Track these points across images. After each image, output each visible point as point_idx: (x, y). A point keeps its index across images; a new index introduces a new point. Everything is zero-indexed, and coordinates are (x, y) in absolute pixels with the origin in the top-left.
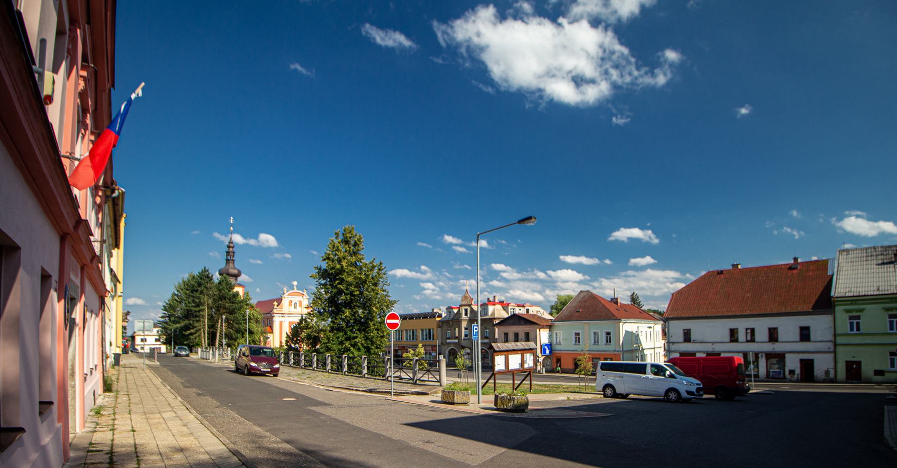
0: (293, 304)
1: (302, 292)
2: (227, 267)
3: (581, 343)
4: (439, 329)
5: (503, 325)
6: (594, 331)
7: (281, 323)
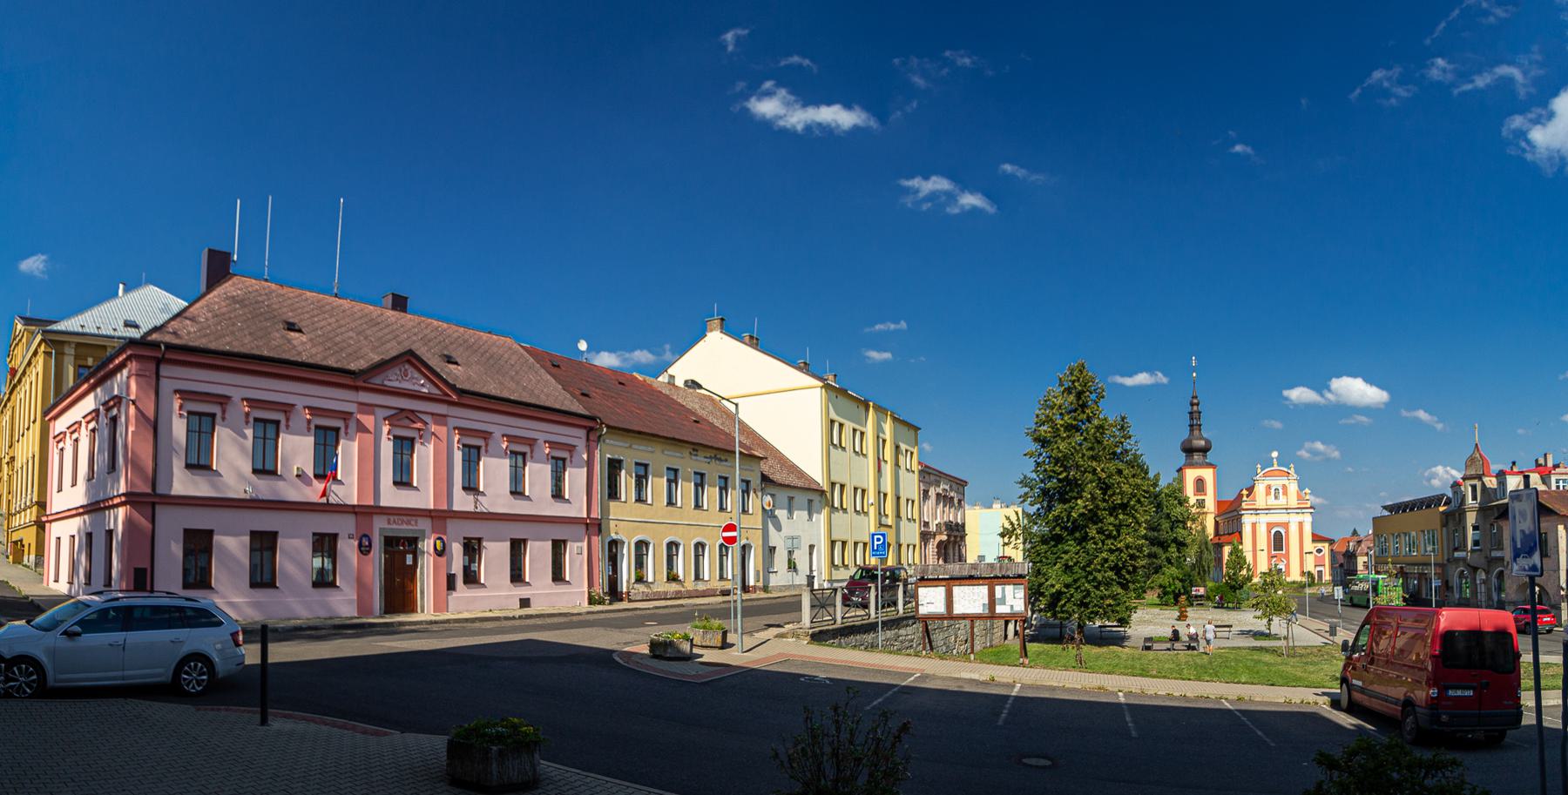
1: (1286, 470)
2: (1191, 437)
4: (1444, 529)
7: (1254, 525)
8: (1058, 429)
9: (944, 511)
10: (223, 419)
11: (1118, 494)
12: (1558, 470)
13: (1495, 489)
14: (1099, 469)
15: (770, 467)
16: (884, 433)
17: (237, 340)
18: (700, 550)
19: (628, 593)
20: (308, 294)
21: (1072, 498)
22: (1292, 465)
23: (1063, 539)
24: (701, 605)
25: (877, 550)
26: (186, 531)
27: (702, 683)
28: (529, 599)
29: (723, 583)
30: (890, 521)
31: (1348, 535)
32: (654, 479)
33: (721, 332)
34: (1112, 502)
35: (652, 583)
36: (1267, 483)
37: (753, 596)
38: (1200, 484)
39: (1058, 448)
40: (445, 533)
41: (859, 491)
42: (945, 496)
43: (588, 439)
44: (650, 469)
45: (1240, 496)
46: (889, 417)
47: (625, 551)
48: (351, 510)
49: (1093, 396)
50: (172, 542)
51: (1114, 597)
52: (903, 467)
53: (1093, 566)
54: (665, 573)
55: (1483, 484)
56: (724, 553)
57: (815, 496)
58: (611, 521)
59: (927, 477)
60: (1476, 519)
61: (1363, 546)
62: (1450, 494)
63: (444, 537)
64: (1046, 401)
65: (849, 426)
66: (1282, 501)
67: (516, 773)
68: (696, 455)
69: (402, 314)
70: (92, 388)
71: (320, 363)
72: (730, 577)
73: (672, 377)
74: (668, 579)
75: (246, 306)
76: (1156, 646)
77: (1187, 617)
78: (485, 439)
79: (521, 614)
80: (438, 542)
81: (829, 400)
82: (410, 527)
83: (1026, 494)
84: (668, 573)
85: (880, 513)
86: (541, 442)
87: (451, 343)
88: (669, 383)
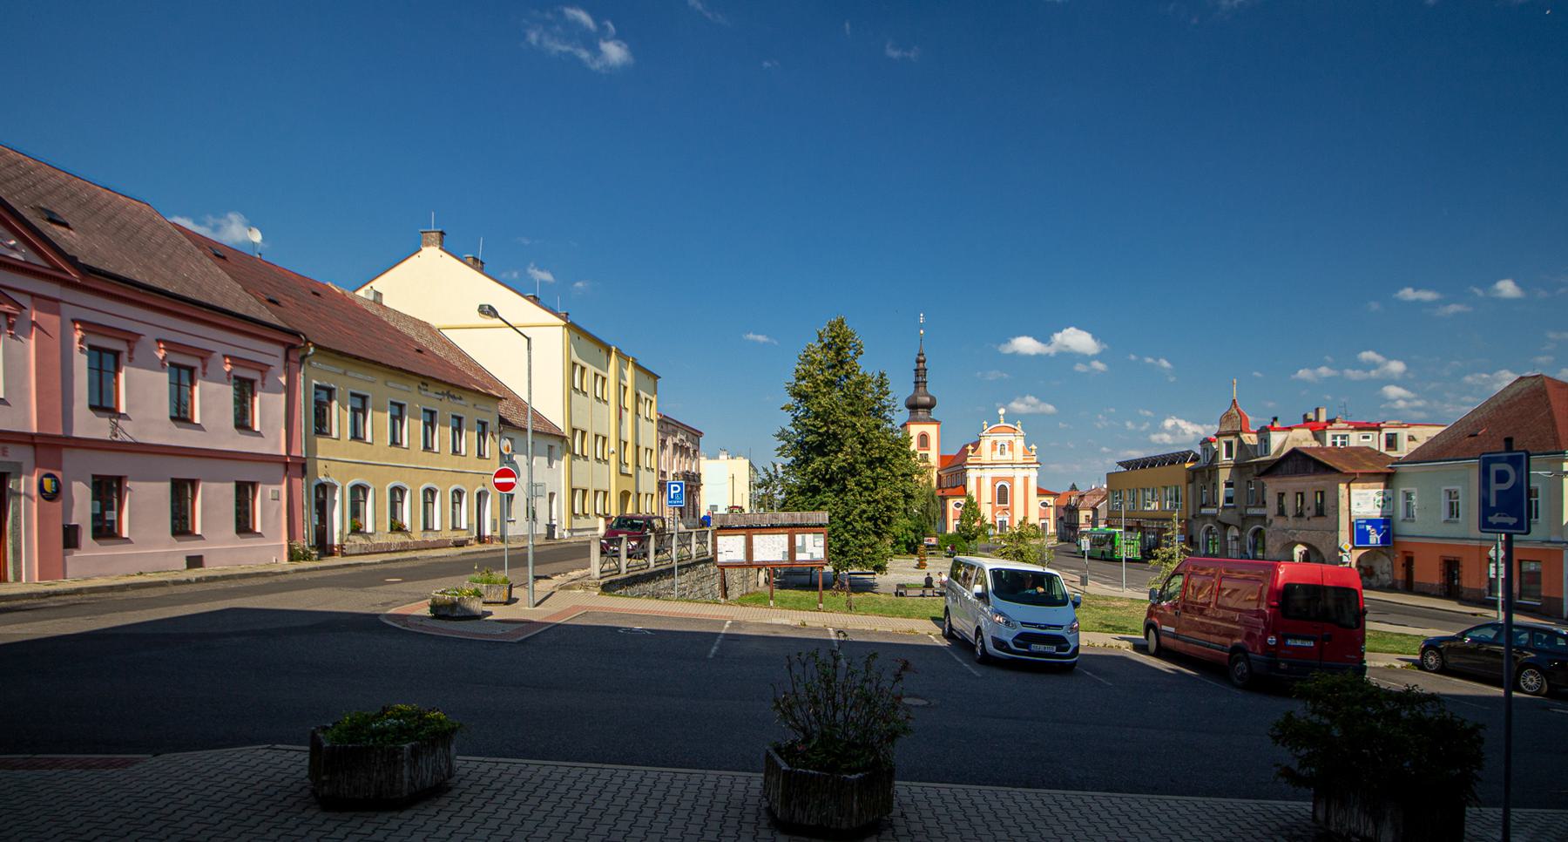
0: (998, 447)
1: (1013, 426)
2: (916, 394)
3: (1460, 519)
4: (1190, 485)
5: (1275, 476)
6: (1404, 489)
7: (979, 479)
8: (818, 384)
12: (1335, 426)
13: (1256, 446)
15: (506, 408)
16: (625, 380)
18: (429, 496)
19: (341, 546)
21: (831, 451)
22: (1019, 422)
23: (820, 490)
24: (437, 557)
25: (674, 499)
27: (519, 642)
28: (201, 557)
29: (456, 533)
30: (630, 470)
31: (1067, 489)
32: (374, 413)
33: (440, 248)
36: (992, 439)
37: (492, 547)
38: (924, 439)
39: (819, 403)
40: (60, 469)
41: (600, 439)
42: (682, 446)
43: (287, 359)
44: (370, 402)
45: (964, 451)
46: (630, 363)
49: (851, 353)
51: (871, 546)
52: (642, 416)
53: (851, 517)
54: (388, 523)
55: (1241, 441)
57: (554, 442)
58: (319, 461)
60: (1230, 476)
61: (1085, 500)
62: (1198, 450)
63: (58, 474)
64: (806, 356)
65: (591, 369)
66: (1008, 456)
67: (430, 775)
72: (464, 526)
73: (378, 294)
74: (392, 529)
76: (910, 593)
77: (926, 565)
79: (199, 576)
80: (47, 482)
81: (571, 341)
83: (783, 446)
84: (392, 522)
85: (620, 462)
86: (218, 356)
88: (374, 301)
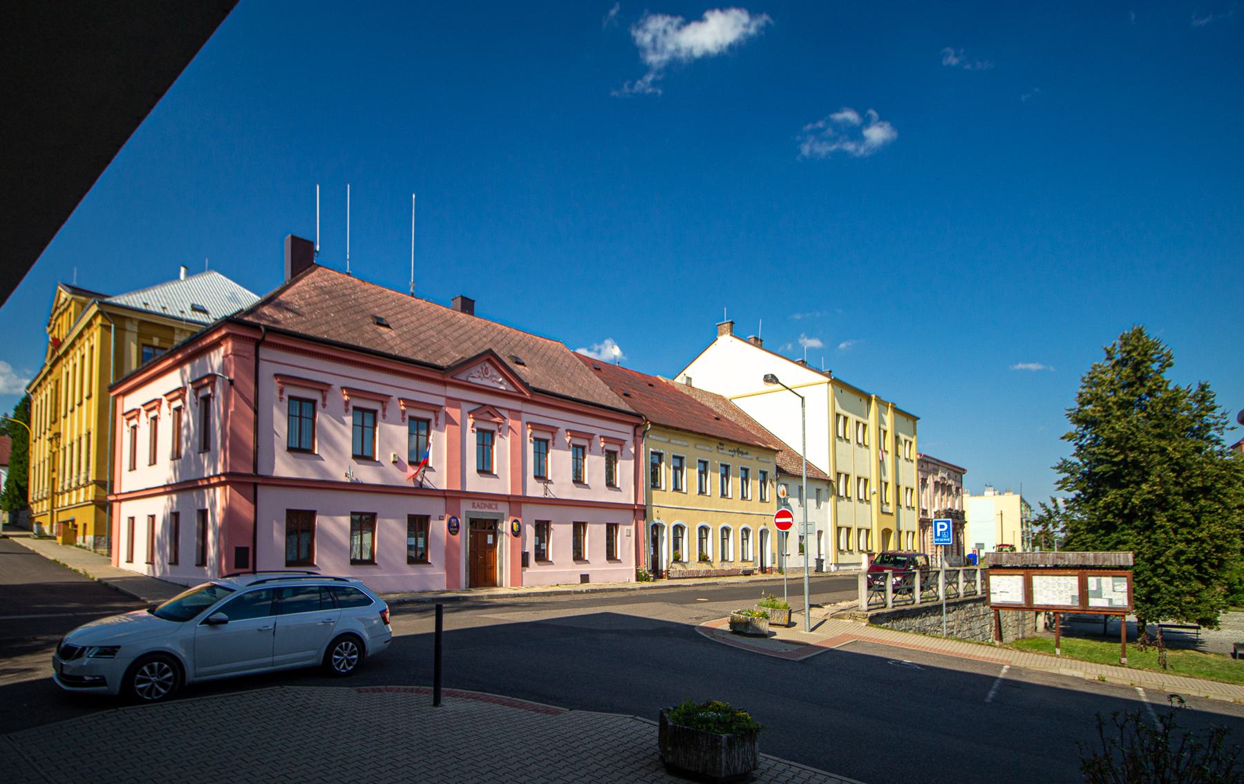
9: (942, 500)
10: (324, 405)
11: (1198, 475)
14: (1170, 449)
16: (885, 424)
17: (333, 329)
19: (667, 571)
20: (389, 291)
25: (940, 537)
26: (289, 511)
29: (744, 564)
30: (891, 509)
34: (1188, 486)
35: (686, 563)
37: (772, 576)
40: (520, 516)
41: (862, 481)
42: (943, 485)
43: (635, 435)
44: (685, 462)
47: (665, 534)
48: (442, 494)
49: (1155, 366)
50: (275, 522)
52: (902, 457)
56: (704, 536)
57: (823, 486)
58: (654, 508)
59: (925, 465)
63: (520, 520)
64: (1092, 378)
65: (853, 418)
68: (722, 449)
69: (471, 316)
70: (179, 364)
71: (411, 358)
73: (689, 379)
74: (700, 560)
75: (335, 298)
78: (552, 433)
80: (515, 524)
81: (835, 394)
82: (492, 511)
83: (1065, 479)
84: (700, 554)
85: (882, 502)
87: (516, 346)
88: (687, 385)
